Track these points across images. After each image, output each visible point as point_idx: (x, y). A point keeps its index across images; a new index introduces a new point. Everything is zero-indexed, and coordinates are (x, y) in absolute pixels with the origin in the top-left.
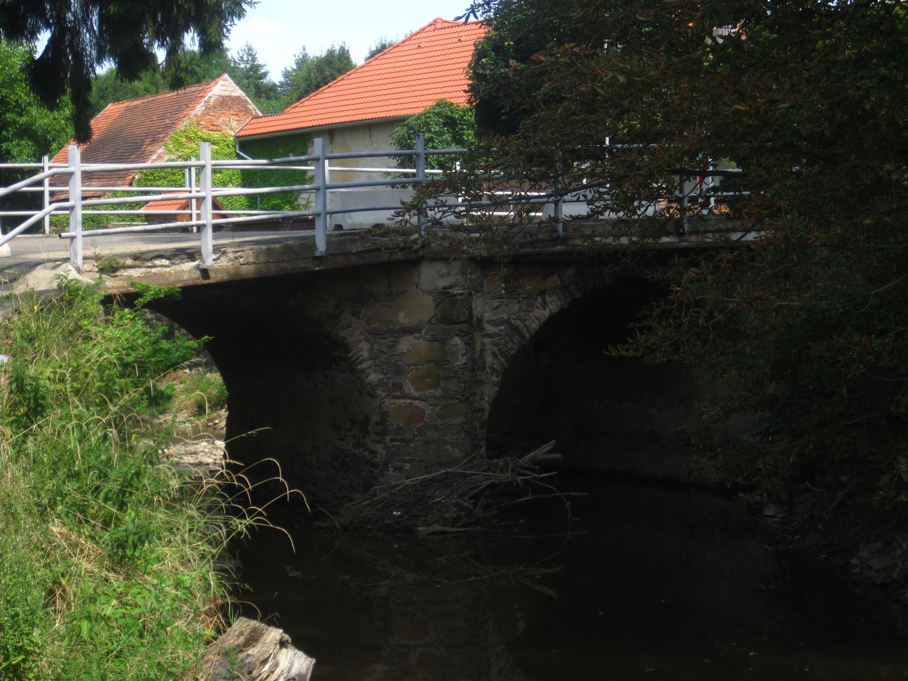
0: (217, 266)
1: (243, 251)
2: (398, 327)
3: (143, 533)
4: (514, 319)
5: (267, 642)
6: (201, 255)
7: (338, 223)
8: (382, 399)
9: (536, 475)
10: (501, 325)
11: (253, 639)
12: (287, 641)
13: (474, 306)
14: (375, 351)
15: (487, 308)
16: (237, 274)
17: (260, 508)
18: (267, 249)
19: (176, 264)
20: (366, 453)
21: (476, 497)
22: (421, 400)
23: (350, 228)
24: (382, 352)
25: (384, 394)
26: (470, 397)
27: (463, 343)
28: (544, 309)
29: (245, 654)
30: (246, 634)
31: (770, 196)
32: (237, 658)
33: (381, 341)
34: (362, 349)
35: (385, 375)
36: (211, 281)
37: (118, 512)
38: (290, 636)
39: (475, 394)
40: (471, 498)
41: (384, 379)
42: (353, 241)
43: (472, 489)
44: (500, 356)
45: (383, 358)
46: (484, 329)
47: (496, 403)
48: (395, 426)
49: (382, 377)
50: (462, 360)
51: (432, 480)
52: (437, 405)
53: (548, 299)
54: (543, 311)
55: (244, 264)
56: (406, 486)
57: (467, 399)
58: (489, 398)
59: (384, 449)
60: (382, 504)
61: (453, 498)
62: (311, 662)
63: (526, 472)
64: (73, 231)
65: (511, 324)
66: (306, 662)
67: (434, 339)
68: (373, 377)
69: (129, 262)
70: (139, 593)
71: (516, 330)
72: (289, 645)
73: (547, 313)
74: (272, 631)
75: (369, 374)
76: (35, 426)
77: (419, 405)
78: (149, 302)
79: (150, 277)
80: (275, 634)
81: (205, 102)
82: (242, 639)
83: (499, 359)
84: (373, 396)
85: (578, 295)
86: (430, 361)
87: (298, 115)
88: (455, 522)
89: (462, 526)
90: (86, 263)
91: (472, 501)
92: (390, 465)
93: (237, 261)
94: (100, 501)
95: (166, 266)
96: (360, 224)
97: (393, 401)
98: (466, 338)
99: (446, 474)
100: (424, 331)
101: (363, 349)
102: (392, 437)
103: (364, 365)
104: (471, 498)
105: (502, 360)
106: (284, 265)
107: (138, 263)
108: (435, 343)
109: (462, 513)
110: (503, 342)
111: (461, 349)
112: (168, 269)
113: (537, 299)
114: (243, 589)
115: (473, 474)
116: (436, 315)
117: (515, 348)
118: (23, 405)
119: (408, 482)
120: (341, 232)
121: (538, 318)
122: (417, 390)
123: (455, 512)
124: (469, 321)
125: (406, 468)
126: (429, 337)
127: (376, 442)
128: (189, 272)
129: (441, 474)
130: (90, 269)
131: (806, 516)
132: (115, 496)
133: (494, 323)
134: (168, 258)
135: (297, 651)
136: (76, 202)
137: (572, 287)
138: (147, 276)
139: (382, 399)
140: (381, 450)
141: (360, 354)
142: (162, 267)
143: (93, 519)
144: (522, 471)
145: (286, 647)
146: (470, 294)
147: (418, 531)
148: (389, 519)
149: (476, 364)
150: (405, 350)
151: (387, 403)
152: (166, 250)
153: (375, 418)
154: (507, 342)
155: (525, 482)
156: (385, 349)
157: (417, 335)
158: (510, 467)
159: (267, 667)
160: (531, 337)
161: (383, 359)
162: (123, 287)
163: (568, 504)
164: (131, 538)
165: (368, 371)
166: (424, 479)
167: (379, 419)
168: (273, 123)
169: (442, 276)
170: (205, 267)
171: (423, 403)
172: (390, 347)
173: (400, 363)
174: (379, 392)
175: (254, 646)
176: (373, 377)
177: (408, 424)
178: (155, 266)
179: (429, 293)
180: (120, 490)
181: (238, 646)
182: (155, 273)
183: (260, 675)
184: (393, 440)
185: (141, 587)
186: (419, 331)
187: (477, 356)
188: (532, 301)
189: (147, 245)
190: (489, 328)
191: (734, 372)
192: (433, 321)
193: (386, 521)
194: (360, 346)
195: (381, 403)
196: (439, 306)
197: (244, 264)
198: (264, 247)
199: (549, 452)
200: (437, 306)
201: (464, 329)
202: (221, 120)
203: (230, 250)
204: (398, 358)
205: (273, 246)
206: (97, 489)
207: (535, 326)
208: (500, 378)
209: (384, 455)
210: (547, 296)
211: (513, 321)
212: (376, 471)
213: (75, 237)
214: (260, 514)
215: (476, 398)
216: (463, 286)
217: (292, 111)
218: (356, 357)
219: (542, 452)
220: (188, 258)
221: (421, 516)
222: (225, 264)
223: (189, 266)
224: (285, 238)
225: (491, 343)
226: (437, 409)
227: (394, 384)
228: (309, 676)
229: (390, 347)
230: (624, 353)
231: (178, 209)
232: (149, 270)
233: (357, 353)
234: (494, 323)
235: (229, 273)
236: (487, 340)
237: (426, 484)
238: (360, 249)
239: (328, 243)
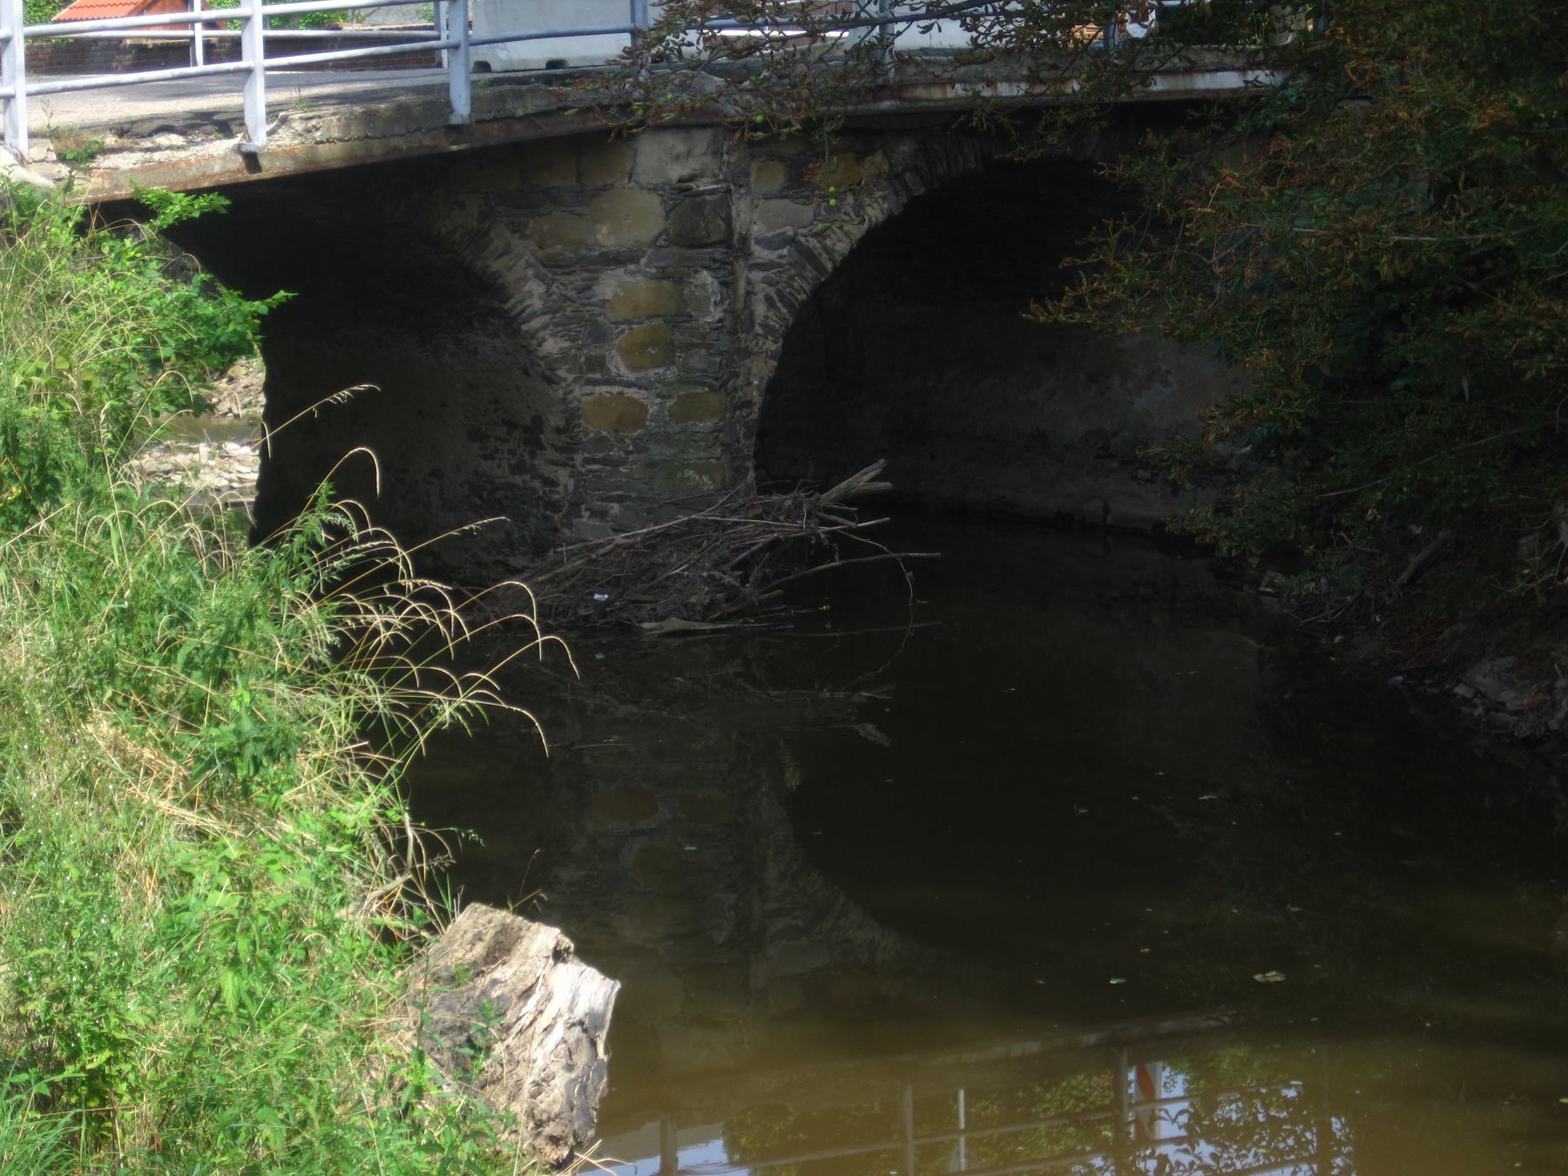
0: (273, 146)
1: (320, 117)
3: (277, 743)
5: (531, 954)
6: (242, 124)
7: (481, 58)
8: (568, 386)
9: (853, 524)
10: (781, 246)
11: (500, 949)
12: (567, 950)
13: (734, 214)
14: (554, 297)
15: (756, 216)
16: (310, 162)
17: (484, 674)
18: (364, 113)
19: (197, 144)
20: (537, 484)
21: (745, 565)
22: (640, 388)
23: (505, 68)
24: (566, 298)
25: (571, 377)
26: (729, 380)
27: (716, 282)
29: (488, 978)
30: (487, 938)
31: (1395, 36)
32: (474, 988)
33: (562, 278)
34: (530, 293)
35: (573, 341)
36: (265, 175)
37: (214, 693)
38: (573, 937)
39: (737, 375)
40: (736, 567)
41: (570, 349)
42: (519, 96)
43: (737, 551)
44: (779, 304)
45: (569, 310)
46: (751, 254)
47: (772, 388)
48: (592, 435)
49: (567, 344)
50: (716, 314)
51: (665, 535)
52: (670, 397)
55: (322, 142)
56: (617, 546)
57: (724, 385)
58: (760, 382)
59: (571, 476)
60: (575, 579)
61: (703, 569)
62: (613, 988)
63: (834, 518)
64: (9, 84)
65: (800, 243)
66: (604, 989)
67: (663, 275)
69: (111, 140)
70: (273, 862)
71: (808, 255)
72: (571, 957)
74: (538, 932)
75: (544, 340)
76: (42, 524)
77: (636, 396)
78: (171, 227)
79: (151, 169)
80: (544, 937)
82: (480, 949)
83: (777, 309)
84: (551, 381)
85: (920, 191)
86: (657, 316)
88: (706, 612)
89: (720, 619)
90: (35, 145)
91: (738, 573)
92: (583, 507)
93: (308, 136)
94: (177, 667)
95: (179, 148)
96: (522, 61)
97: (588, 389)
98: (722, 273)
99: (690, 523)
100: (644, 261)
101: (532, 293)
102: (586, 455)
103: (535, 324)
104: (736, 567)
105: (784, 310)
106: (394, 142)
107: (126, 142)
108: (666, 284)
109: (719, 595)
110: (785, 277)
111: (714, 293)
112: (182, 154)
114: (465, 840)
115: (736, 524)
116: (666, 231)
117: (807, 288)
118: (17, 480)
119: (620, 539)
120: (488, 76)
122: (632, 368)
123: (708, 593)
124: (726, 241)
125: (612, 512)
126: (654, 271)
128: (223, 158)
129: (679, 524)
130: (42, 157)
131: (1349, 598)
132: (208, 660)
133: (768, 244)
134: (182, 133)
135: (583, 966)
136: (13, 29)
137: (908, 176)
138: (146, 168)
139: (568, 386)
141: (528, 302)
142: (173, 151)
143: (165, 705)
144: (826, 516)
145: (565, 961)
146: (728, 191)
147: (642, 629)
148: (586, 607)
149: (738, 321)
150: (609, 296)
151: (577, 392)
152: (174, 116)
153: (555, 420)
154: (792, 278)
155: (833, 536)
156: (571, 294)
157: (631, 267)
158: (805, 510)
159: (532, 1003)
160: (835, 268)
161: (568, 312)
162: (101, 190)
163: (909, 575)
164: (250, 750)
165: (541, 334)
166: (648, 533)
167: (561, 423)
169: (677, 158)
170: (253, 150)
173: (600, 319)
174: (562, 373)
175: (504, 963)
176: (552, 346)
177: (616, 431)
178: (158, 149)
179: (655, 189)
180: (218, 648)
181: (474, 963)
182: (160, 162)
183: (519, 1019)
184: (587, 461)
185: (276, 848)
186: (635, 260)
187: (740, 305)
189: (136, 104)
190: (761, 253)
191: (1265, 351)
192: (661, 242)
193: (582, 612)
194: (526, 289)
196: (672, 214)
197: (322, 142)
198: (358, 109)
199: (873, 480)
200: (668, 213)
201: (718, 256)
203: (297, 116)
204: (597, 310)
205: (373, 106)
206: (171, 646)
207: (842, 247)
208: (780, 344)
209: (571, 488)
211: (803, 239)
212: (557, 517)
213: (13, 97)
214: (485, 685)
215: (740, 382)
216: (715, 176)
218: (519, 309)
219: (863, 480)
220: (220, 131)
221: (646, 602)
222: (287, 142)
223: (220, 147)
224: (391, 89)
226: (670, 403)
227: (589, 359)
228: (609, 1015)
229: (582, 290)
230: (1062, 317)
231: (130, 14)
232: (148, 155)
233: (521, 302)
234: (768, 244)
235: (295, 158)
236: (757, 275)
237: (653, 543)
238: (530, 111)
239: (475, 100)
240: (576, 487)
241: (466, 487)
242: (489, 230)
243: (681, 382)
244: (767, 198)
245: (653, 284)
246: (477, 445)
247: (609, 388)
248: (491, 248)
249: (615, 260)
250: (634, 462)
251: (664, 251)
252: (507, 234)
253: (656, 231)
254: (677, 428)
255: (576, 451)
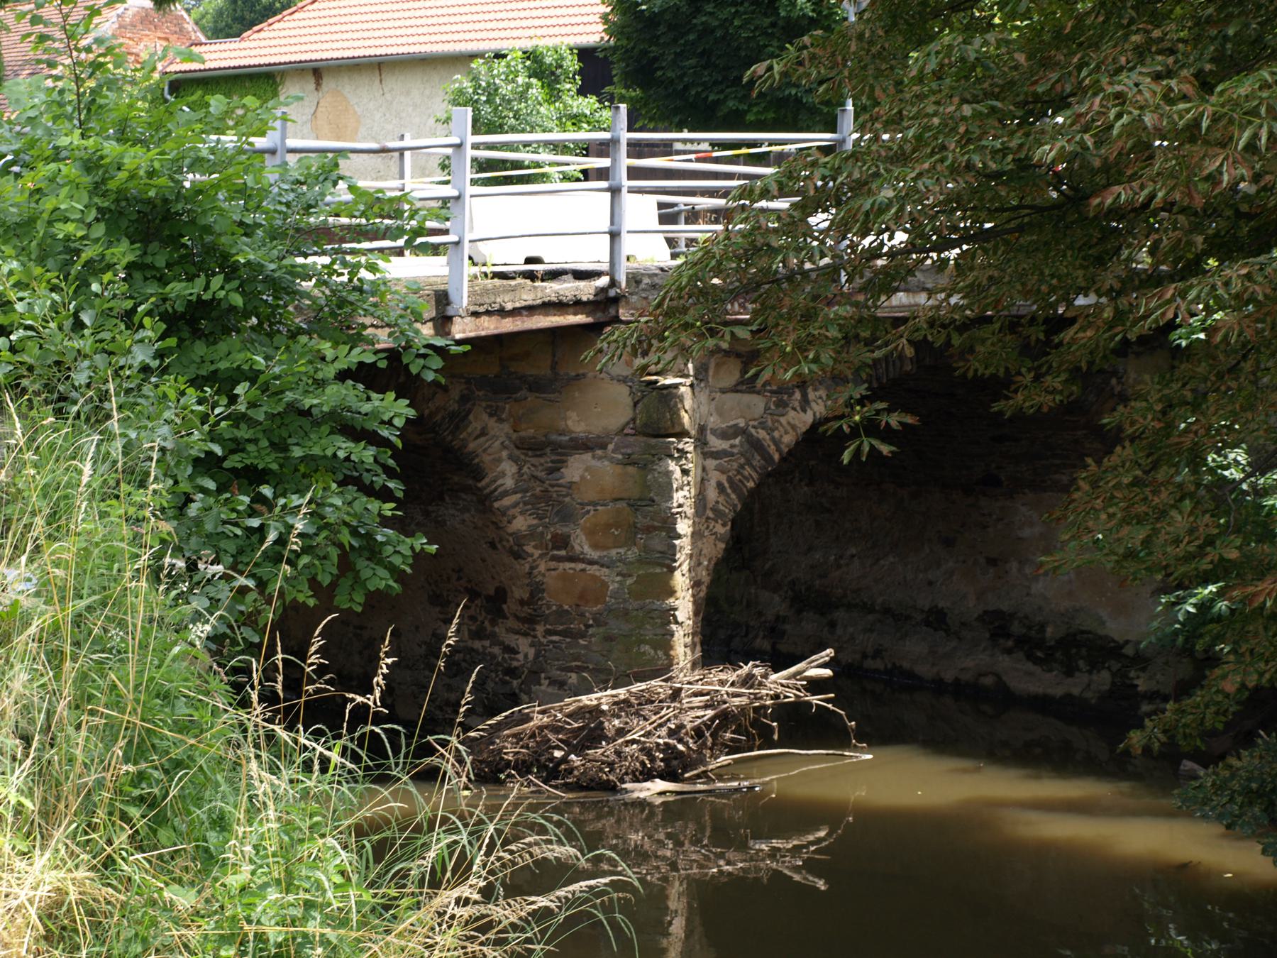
2: (567, 438)
4: (754, 427)
20: (496, 650)
22: (602, 566)
25: (537, 553)
28: (804, 411)
33: (534, 460)
35: (541, 519)
44: (729, 491)
48: (554, 608)
49: (535, 522)
53: (811, 395)
54: (802, 414)
58: (709, 561)
59: (532, 645)
67: (629, 461)
68: (521, 523)
71: (756, 445)
73: (808, 418)
75: (515, 517)
77: (598, 574)
81: (119, 16)
83: (728, 495)
84: (518, 555)
87: (262, 43)
92: (543, 675)
97: (553, 564)
100: (611, 447)
101: (506, 474)
103: (507, 501)
105: (733, 496)
108: (631, 469)
110: (735, 465)
113: (793, 393)
116: (634, 420)
121: (794, 427)
122: (595, 546)
126: (620, 457)
127: (517, 633)
140: (525, 648)
150: (576, 479)
151: (542, 568)
153: (519, 592)
154: (742, 467)
156: (542, 475)
157: (599, 452)
167: (526, 596)
168: (233, 54)
171: (605, 570)
172: (551, 471)
173: (567, 499)
174: (529, 549)
176: (521, 523)
186: (603, 446)
188: (785, 397)
195: (532, 568)
196: (640, 405)
202: (141, 46)
204: (564, 491)
207: (788, 439)
208: (728, 527)
209: (531, 656)
210: (810, 390)
211: (753, 431)
212: (515, 683)
217: (256, 36)
225: (717, 469)
226: (629, 581)
227: (555, 536)
233: (495, 481)
234: (724, 435)
240: (537, 656)
241: (424, 647)
242: (469, 412)
243: (641, 561)
244: (723, 391)
245: (619, 469)
246: (438, 609)
247: (572, 565)
248: (469, 430)
249: (584, 445)
250: (592, 636)
251: (631, 439)
252: (485, 416)
253: (624, 420)
254: (636, 604)
255: (538, 623)
